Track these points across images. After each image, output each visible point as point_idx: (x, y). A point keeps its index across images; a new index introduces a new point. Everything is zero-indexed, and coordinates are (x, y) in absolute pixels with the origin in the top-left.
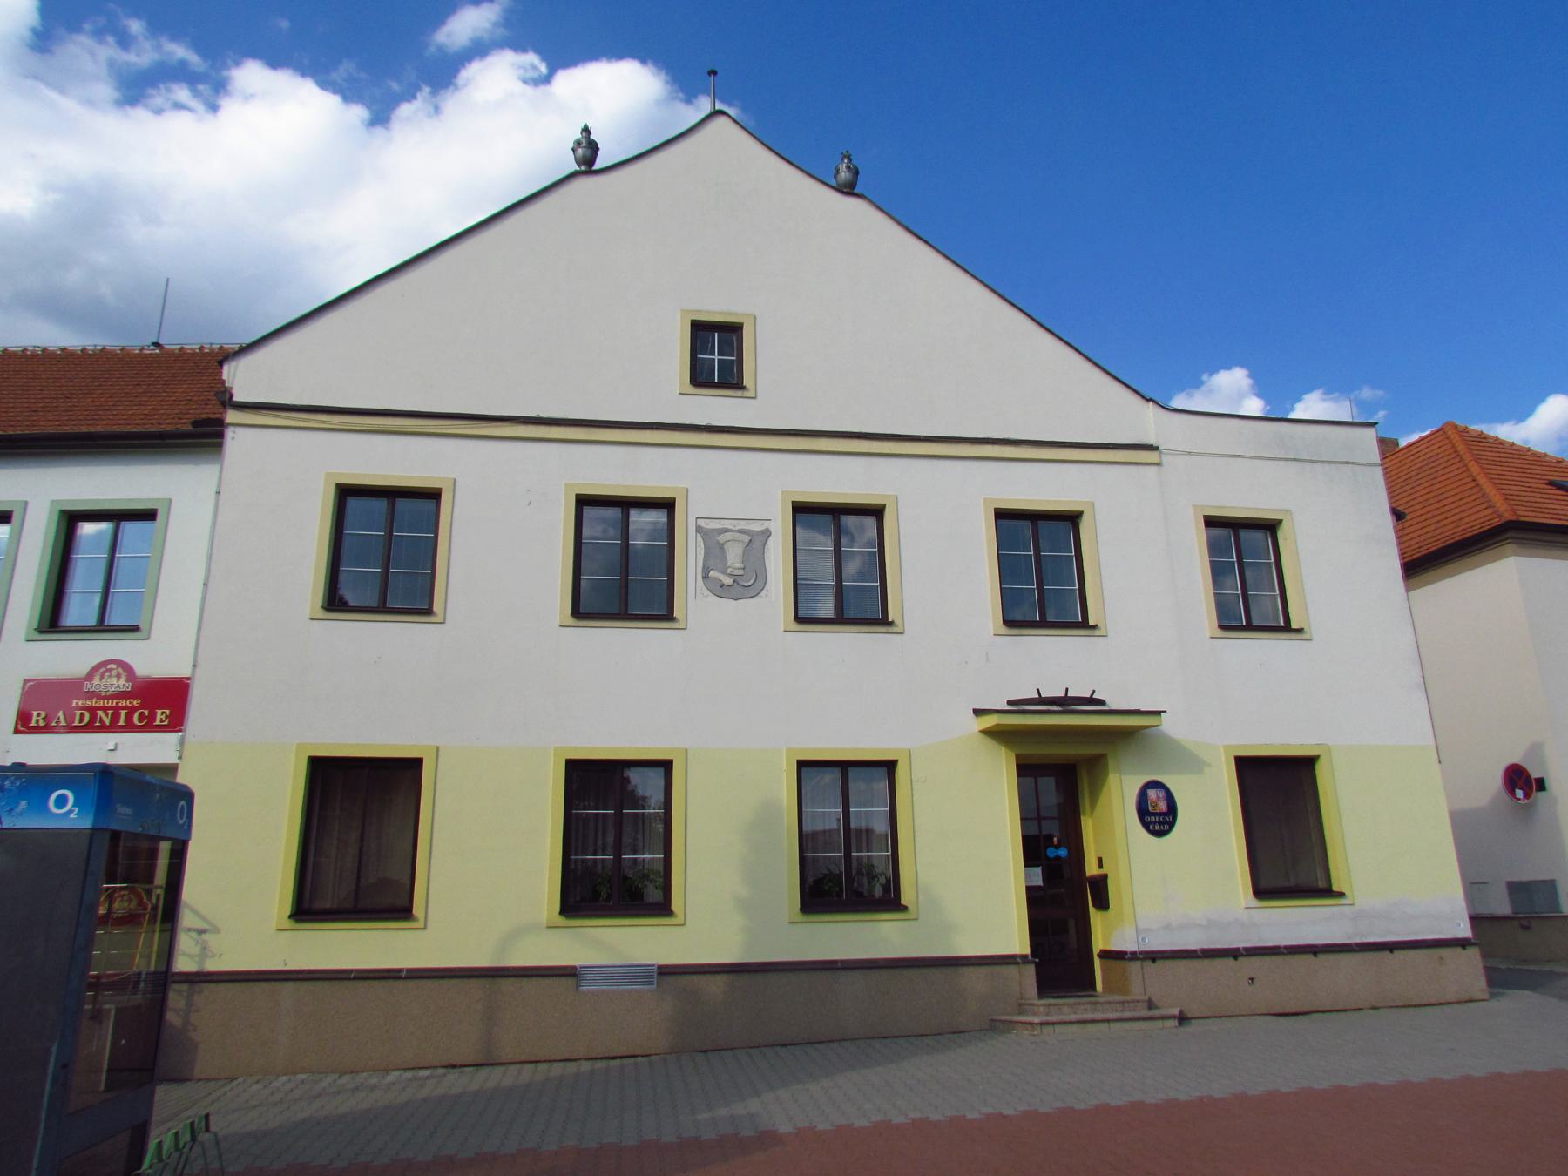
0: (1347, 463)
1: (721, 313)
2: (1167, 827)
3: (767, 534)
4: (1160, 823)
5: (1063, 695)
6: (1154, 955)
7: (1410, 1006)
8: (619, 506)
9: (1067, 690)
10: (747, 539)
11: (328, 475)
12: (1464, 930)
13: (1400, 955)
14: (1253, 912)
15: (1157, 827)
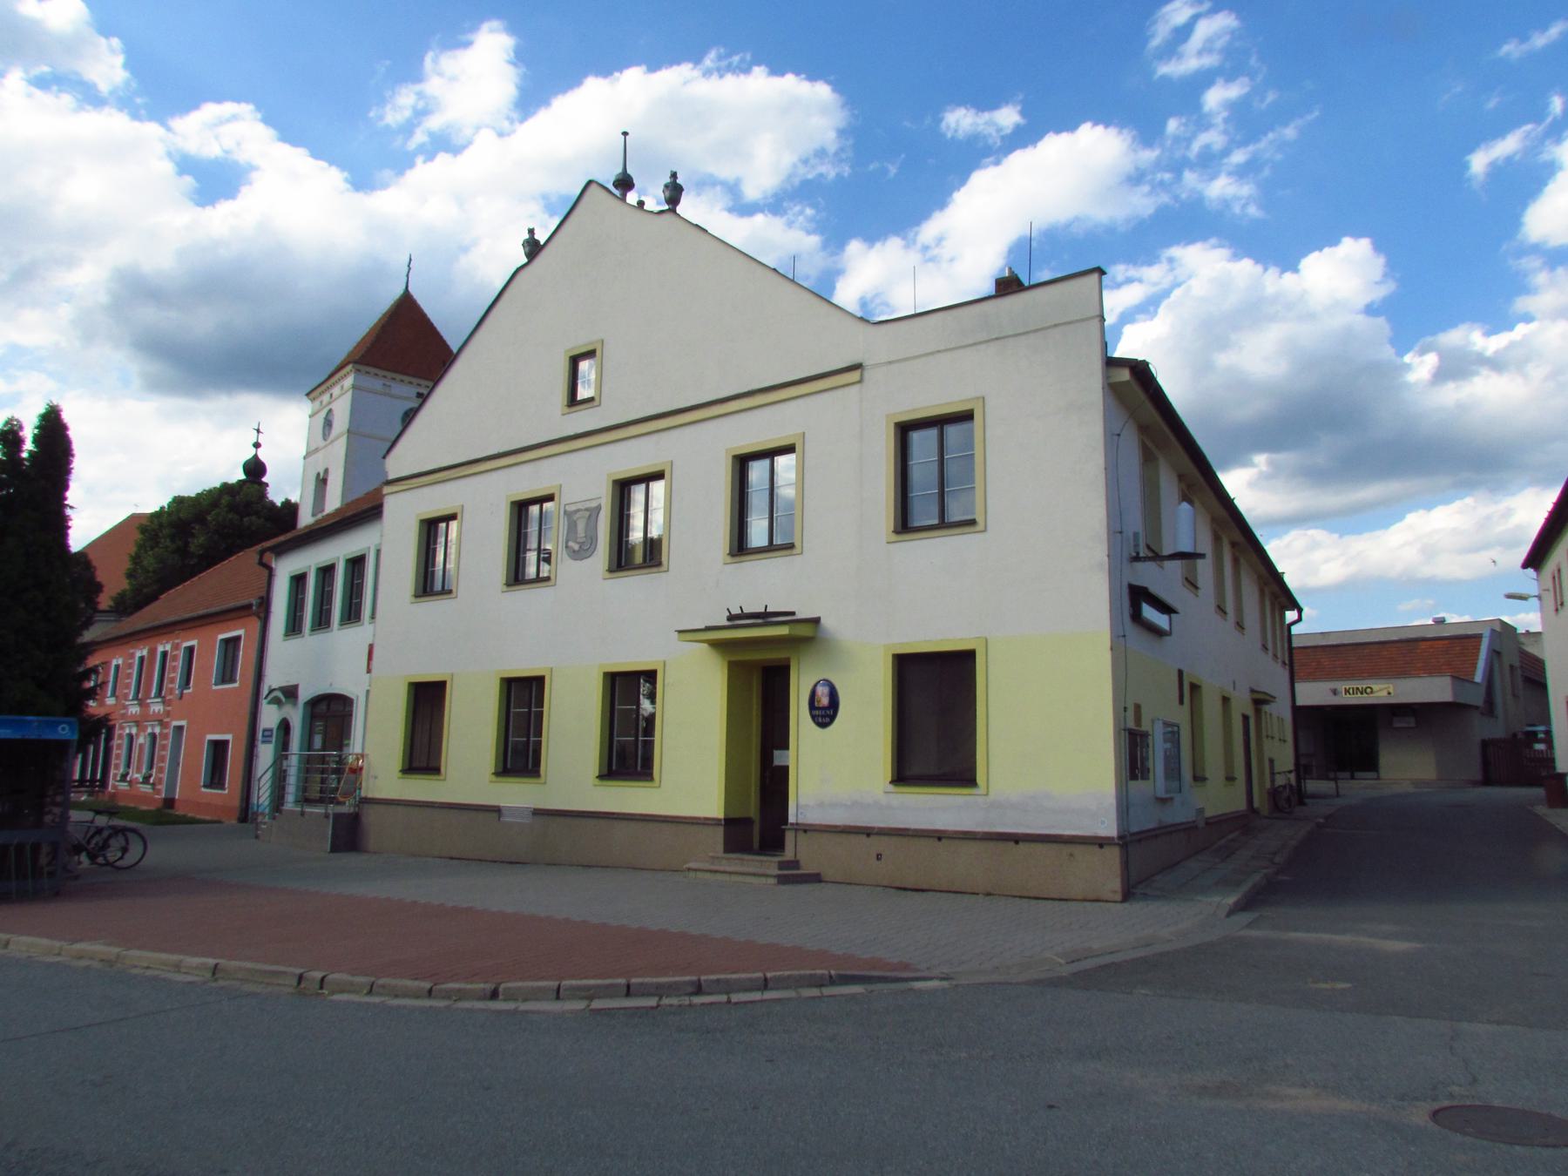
0: (1056, 325)
1: (586, 345)
2: (828, 720)
3: (599, 508)
4: (823, 716)
5: (763, 610)
6: (807, 828)
7: (950, 892)
8: (767, 457)
9: (766, 607)
10: (587, 514)
11: (887, 416)
12: (1109, 828)
13: (1023, 847)
14: (892, 796)
15: (820, 720)
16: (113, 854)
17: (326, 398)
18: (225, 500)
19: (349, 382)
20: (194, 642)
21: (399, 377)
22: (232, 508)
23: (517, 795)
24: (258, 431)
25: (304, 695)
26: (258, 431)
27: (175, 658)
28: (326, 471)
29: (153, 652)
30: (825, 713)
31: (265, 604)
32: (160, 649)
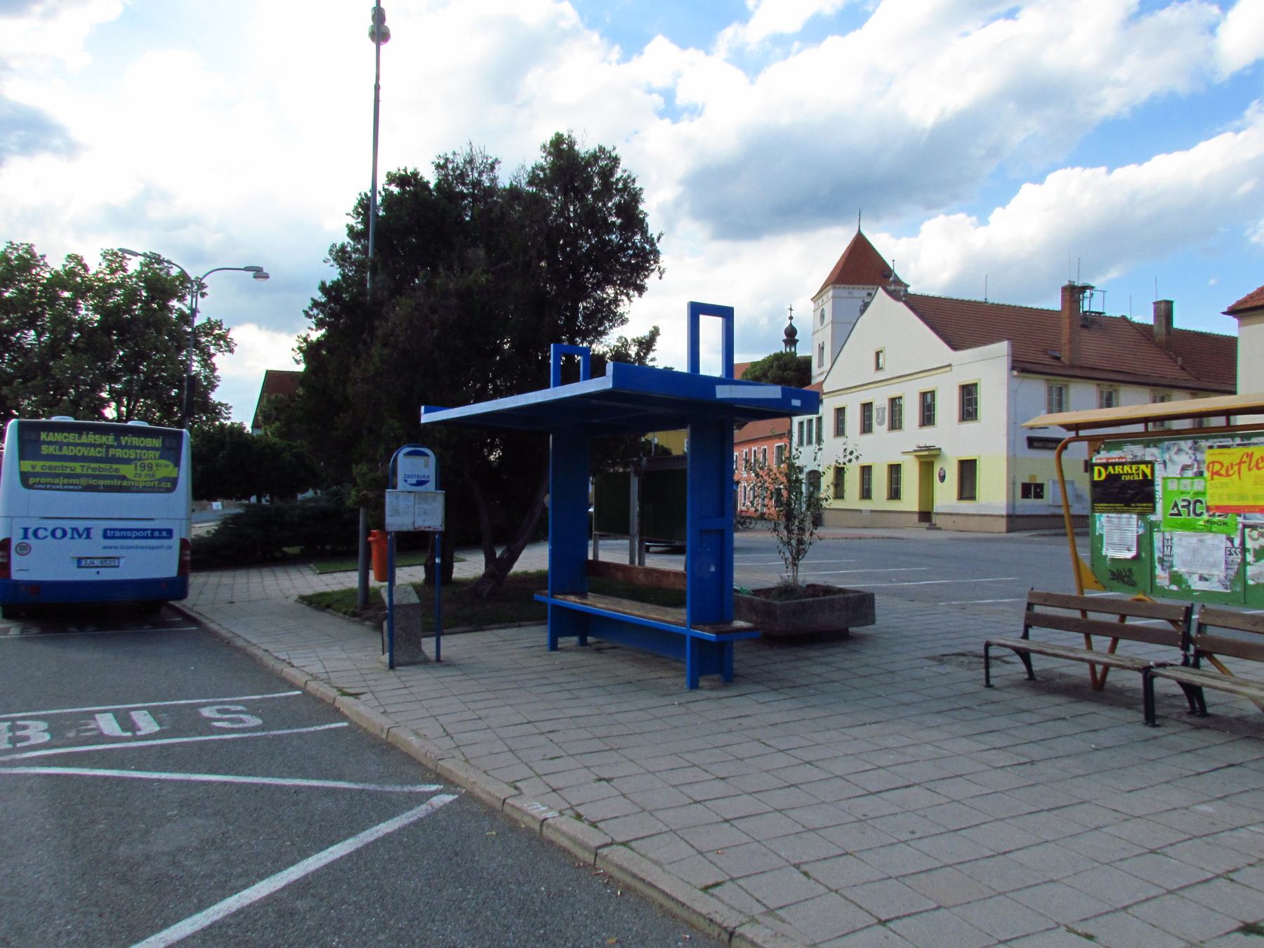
16: (748, 525)
17: (820, 301)
18: (776, 363)
19: (830, 294)
20: (766, 447)
21: (856, 286)
22: (779, 368)
23: (866, 505)
24: (791, 309)
25: (806, 470)
26: (791, 309)
27: (759, 453)
28: (823, 343)
29: (750, 450)
30: (942, 478)
31: (790, 432)
32: (753, 449)
